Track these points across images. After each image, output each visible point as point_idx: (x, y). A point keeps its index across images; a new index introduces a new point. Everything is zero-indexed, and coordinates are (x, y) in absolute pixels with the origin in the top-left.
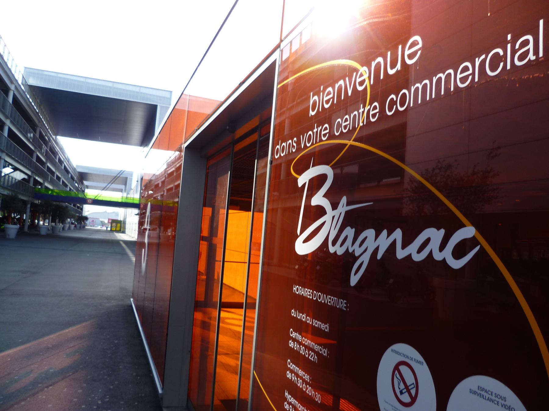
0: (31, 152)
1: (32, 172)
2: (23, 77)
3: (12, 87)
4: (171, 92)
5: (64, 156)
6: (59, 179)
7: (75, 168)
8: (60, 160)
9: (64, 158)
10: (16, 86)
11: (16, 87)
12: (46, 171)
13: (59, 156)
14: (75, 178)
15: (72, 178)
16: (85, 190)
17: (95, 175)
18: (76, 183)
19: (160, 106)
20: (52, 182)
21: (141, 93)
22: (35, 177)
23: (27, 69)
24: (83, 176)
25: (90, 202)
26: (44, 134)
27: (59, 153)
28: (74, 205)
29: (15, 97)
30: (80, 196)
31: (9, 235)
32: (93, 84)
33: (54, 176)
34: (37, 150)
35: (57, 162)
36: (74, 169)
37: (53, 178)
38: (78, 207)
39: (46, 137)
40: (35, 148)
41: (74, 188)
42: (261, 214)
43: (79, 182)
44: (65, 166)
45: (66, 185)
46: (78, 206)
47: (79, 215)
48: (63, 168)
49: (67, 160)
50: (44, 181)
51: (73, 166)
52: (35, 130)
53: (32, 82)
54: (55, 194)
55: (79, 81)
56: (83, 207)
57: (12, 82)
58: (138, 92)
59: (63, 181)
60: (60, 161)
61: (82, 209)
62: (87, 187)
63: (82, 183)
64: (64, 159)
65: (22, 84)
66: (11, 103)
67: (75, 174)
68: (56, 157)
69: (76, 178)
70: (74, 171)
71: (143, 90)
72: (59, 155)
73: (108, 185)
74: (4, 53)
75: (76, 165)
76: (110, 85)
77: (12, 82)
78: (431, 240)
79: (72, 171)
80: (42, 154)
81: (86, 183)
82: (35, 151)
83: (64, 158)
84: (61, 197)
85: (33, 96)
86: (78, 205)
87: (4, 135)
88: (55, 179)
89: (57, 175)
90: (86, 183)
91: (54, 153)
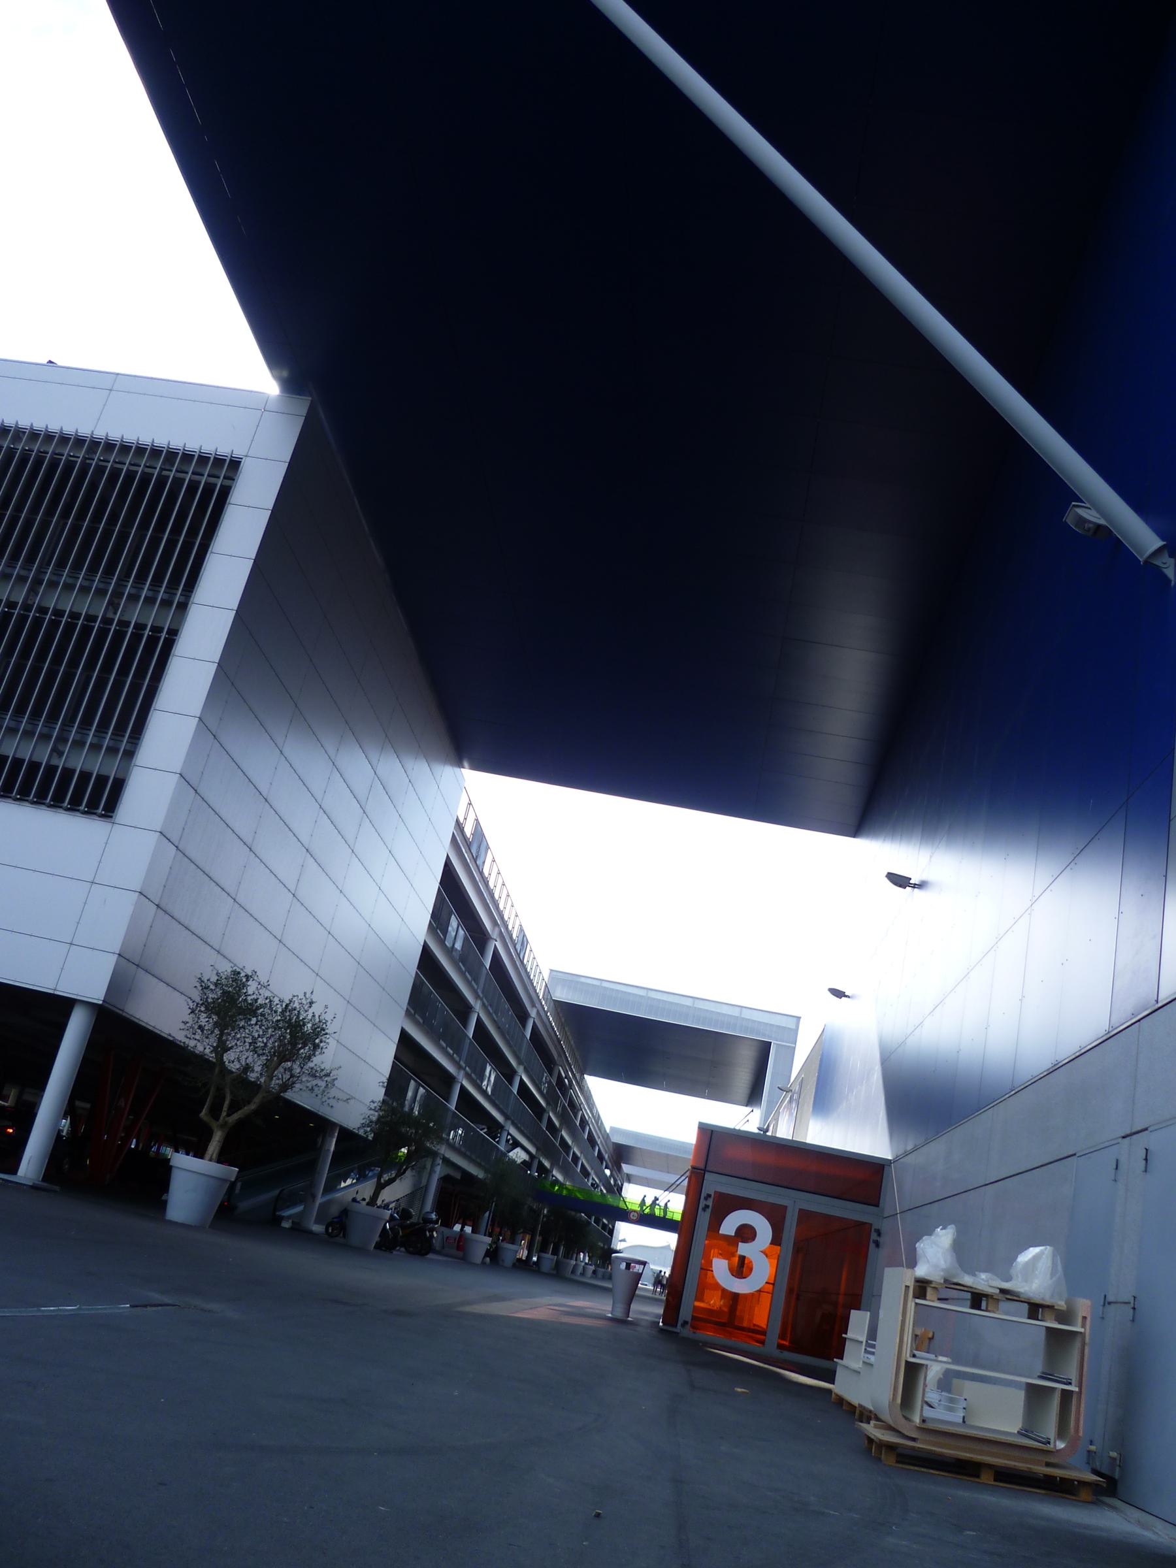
0: (539, 1111)
1: (538, 1149)
2: (546, 985)
3: (533, 1013)
4: (799, 1018)
5: (591, 1111)
6: (576, 1159)
7: (608, 1134)
8: (583, 1117)
9: (590, 1115)
10: (538, 1011)
11: (538, 1012)
12: (558, 1145)
13: (590, 1128)
14: (606, 1157)
15: (600, 1157)
16: (622, 1185)
17: (650, 1153)
18: (605, 1168)
19: (775, 1046)
20: (566, 1171)
21: (743, 1019)
22: (541, 1159)
23: (554, 973)
24: (621, 1154)
25: (635, 1218)
26: (564, 1075)
27: (589, 1122)
28: (597, 1222)
29: (535, 1026)
30: (610, 1200)
31: (503, 1260)
32: (659, 1000)
33: (540, 1119)
34: (551, 1107)
35: (578, 1125)
36: (607, 1137)
37: (566, 1159)
38: (604, 1227)
39: (566, 1080)
40: (548, 1103)
41: (600, 1181)
42: (1026, 1315)
43: (613, 1166)
44: (590, 1132)
45: (585, 1173)
46: (604, 1223)
47: (604, 1247)
48: (596, 1155)
49: (595, 1120)
50: (552, 1165)
51: (605, 1131)
52: (551, 1072)
53: (561, 995)
54: (565, 1192)
55: (636, 995)
56: (614, 1227)
57: (533, 1005)
58: (736, 1018)
59: (582, 1164)
60: (584, 1122)
61: (611, 1232)
62: (629, 1179)
63: (619, 1169)
64: (589, 1117)
65: (543, 997)
66: (528, 1038)
67: (606, 1147)
68: (576, 1117)
69: (609, 1157)
70: (606, 1142)
71: (746, 1015)
72: (591, 1126)
73: (680, 1178)
74: (509, 918)
75: (611, 1127)
76: (689, 1002)
77: (533, 1005)
78: (753, 1273)
79: (601, 1141)
80: (555, 1113)
81: (626, 1168)
82: (547, 1110)
83: (590, 1115)
84: (576, 1200)
85: (557, 1016)
86: (605, 1221)
87: (468, 1034)
88: (570, 1160)
89: (574, 1153)
90: (626, 1168)
91: (574, 1106)
